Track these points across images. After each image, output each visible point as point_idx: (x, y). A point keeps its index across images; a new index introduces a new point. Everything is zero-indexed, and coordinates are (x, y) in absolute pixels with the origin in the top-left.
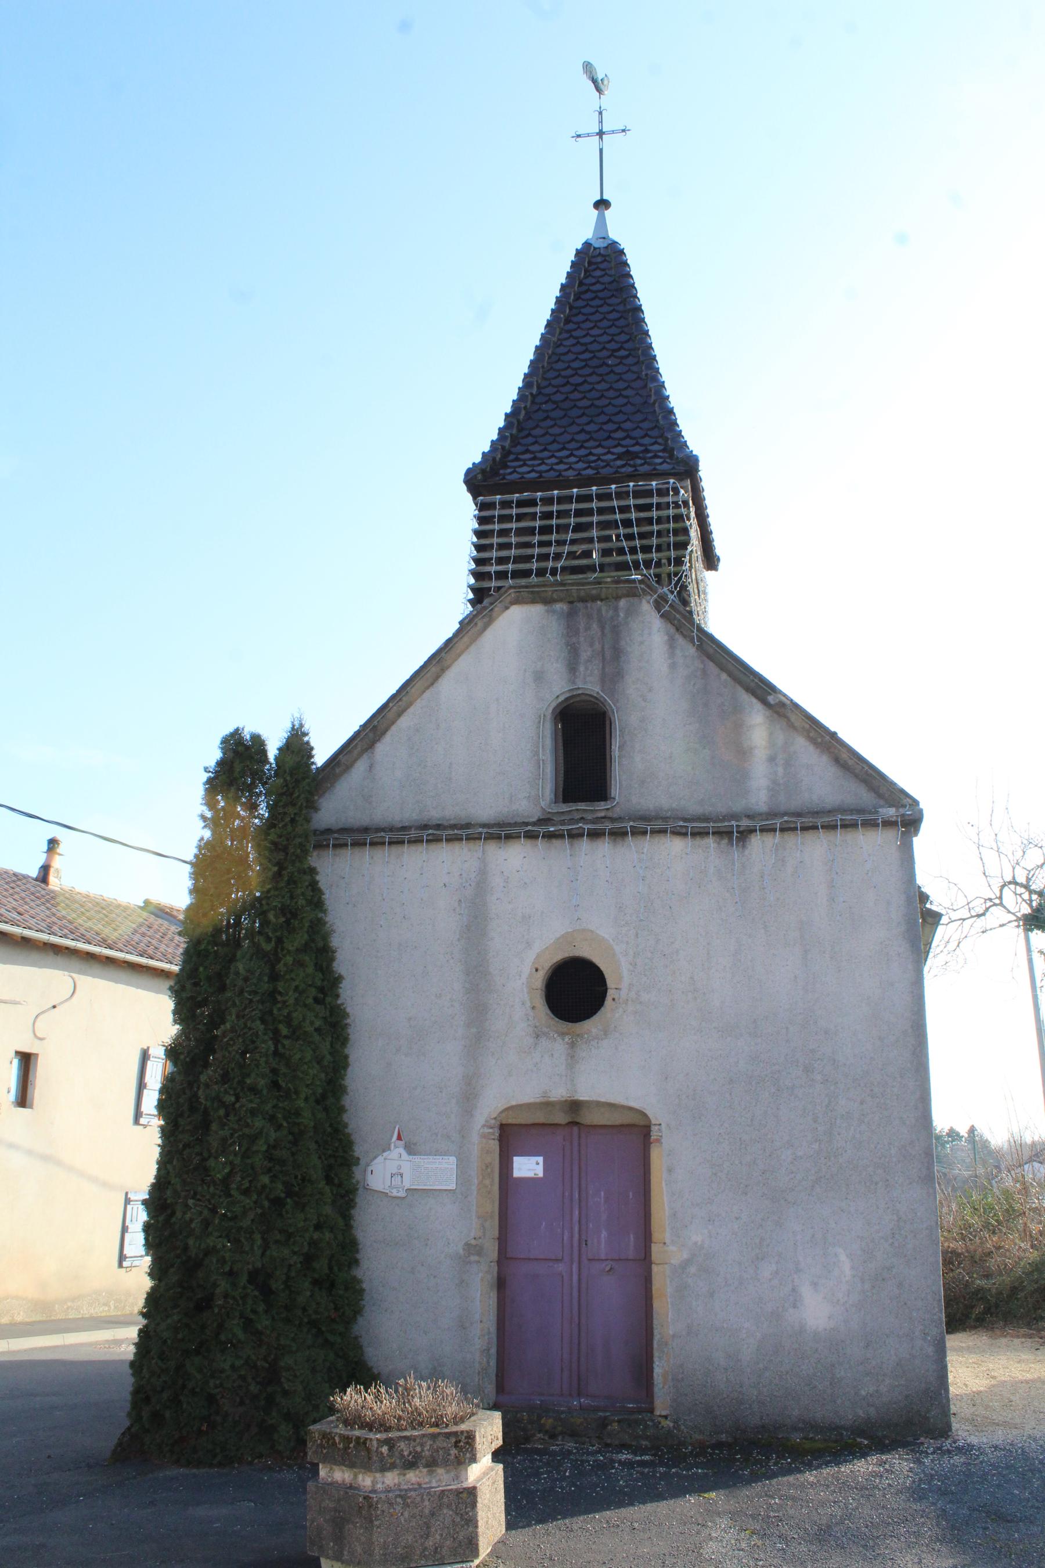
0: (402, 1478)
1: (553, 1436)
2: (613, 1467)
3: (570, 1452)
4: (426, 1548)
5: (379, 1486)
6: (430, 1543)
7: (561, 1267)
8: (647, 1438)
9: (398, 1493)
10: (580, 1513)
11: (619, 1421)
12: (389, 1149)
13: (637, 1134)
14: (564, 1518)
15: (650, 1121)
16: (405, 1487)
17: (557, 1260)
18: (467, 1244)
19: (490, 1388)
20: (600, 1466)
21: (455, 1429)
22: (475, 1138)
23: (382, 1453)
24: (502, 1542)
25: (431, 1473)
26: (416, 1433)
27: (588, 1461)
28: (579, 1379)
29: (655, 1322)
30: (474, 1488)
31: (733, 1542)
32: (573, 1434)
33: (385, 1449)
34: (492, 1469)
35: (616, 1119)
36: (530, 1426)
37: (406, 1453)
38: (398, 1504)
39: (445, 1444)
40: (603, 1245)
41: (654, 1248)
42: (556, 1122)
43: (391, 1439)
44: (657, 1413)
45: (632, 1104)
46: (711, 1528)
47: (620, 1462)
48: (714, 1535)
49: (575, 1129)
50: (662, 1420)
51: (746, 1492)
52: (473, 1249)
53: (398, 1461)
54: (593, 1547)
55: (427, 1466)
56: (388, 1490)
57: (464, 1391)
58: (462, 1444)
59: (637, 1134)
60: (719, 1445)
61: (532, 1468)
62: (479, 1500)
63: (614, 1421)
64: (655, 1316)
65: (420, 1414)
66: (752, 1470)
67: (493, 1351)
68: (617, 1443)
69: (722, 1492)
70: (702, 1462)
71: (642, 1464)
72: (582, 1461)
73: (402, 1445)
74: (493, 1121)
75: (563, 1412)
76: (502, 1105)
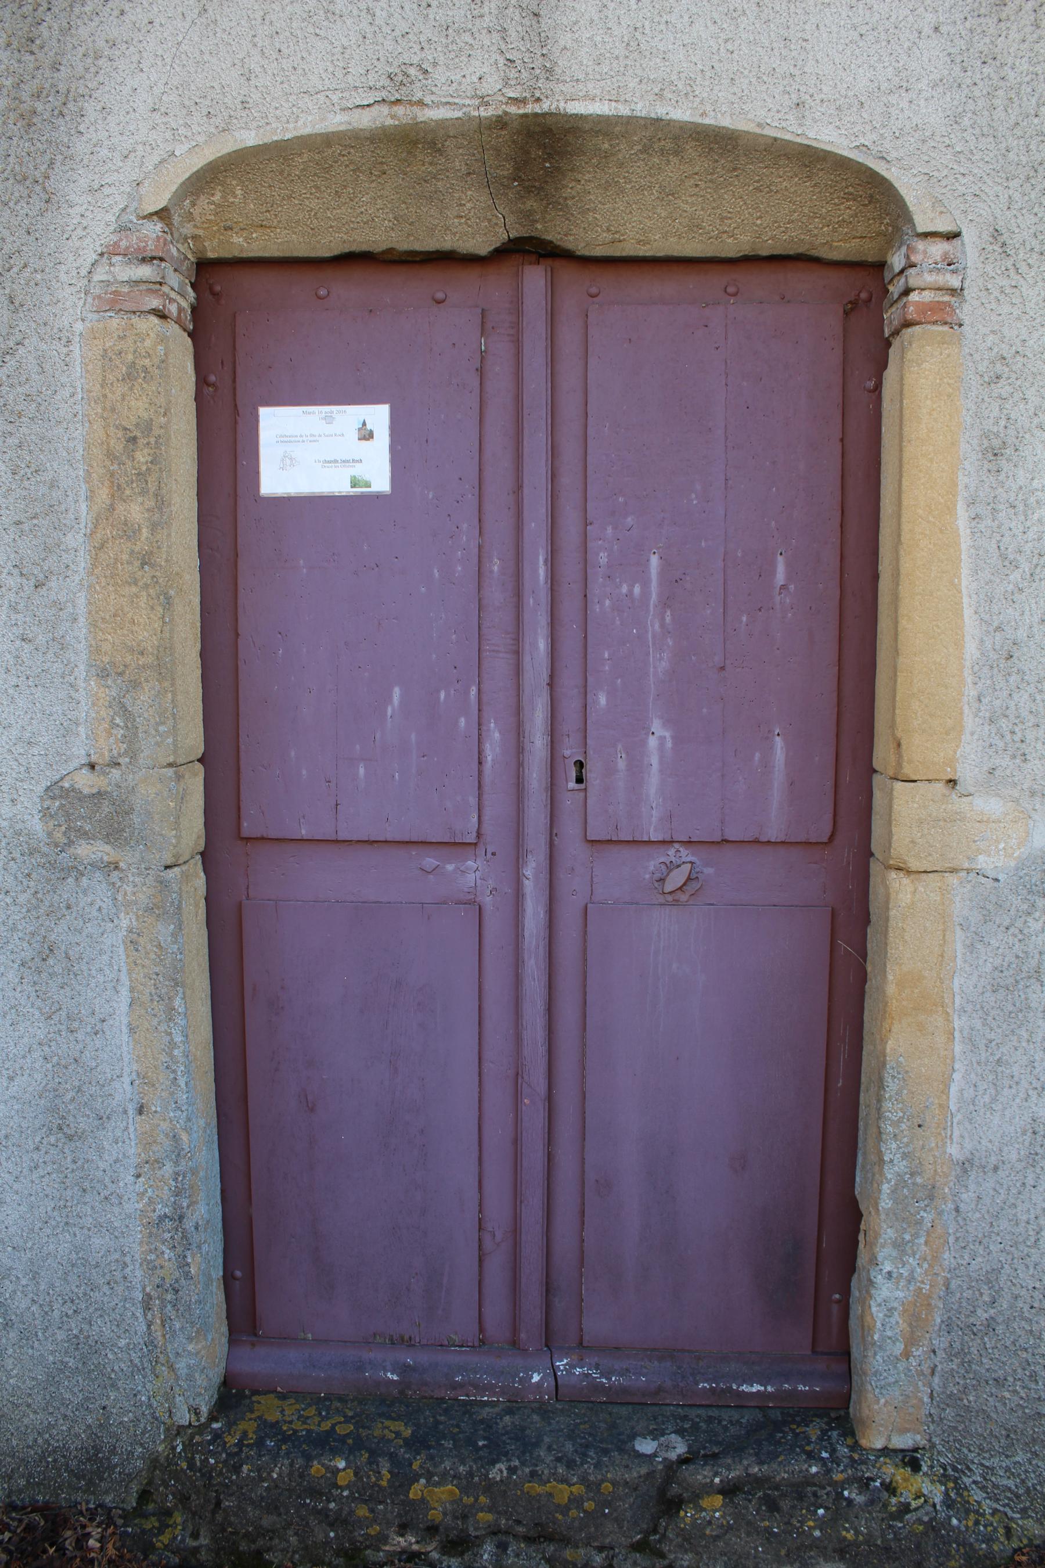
7: (472, 874)
11: (729, 1491)
17: (455, 846)
18: (56, 791)
28: (549, 1289)
36: (362, 1511)
42: (447, 243)
45: (828, 135)
49: (535, 278)
52: (87, 813)
63: (709, 1489)
74: (155, 228)
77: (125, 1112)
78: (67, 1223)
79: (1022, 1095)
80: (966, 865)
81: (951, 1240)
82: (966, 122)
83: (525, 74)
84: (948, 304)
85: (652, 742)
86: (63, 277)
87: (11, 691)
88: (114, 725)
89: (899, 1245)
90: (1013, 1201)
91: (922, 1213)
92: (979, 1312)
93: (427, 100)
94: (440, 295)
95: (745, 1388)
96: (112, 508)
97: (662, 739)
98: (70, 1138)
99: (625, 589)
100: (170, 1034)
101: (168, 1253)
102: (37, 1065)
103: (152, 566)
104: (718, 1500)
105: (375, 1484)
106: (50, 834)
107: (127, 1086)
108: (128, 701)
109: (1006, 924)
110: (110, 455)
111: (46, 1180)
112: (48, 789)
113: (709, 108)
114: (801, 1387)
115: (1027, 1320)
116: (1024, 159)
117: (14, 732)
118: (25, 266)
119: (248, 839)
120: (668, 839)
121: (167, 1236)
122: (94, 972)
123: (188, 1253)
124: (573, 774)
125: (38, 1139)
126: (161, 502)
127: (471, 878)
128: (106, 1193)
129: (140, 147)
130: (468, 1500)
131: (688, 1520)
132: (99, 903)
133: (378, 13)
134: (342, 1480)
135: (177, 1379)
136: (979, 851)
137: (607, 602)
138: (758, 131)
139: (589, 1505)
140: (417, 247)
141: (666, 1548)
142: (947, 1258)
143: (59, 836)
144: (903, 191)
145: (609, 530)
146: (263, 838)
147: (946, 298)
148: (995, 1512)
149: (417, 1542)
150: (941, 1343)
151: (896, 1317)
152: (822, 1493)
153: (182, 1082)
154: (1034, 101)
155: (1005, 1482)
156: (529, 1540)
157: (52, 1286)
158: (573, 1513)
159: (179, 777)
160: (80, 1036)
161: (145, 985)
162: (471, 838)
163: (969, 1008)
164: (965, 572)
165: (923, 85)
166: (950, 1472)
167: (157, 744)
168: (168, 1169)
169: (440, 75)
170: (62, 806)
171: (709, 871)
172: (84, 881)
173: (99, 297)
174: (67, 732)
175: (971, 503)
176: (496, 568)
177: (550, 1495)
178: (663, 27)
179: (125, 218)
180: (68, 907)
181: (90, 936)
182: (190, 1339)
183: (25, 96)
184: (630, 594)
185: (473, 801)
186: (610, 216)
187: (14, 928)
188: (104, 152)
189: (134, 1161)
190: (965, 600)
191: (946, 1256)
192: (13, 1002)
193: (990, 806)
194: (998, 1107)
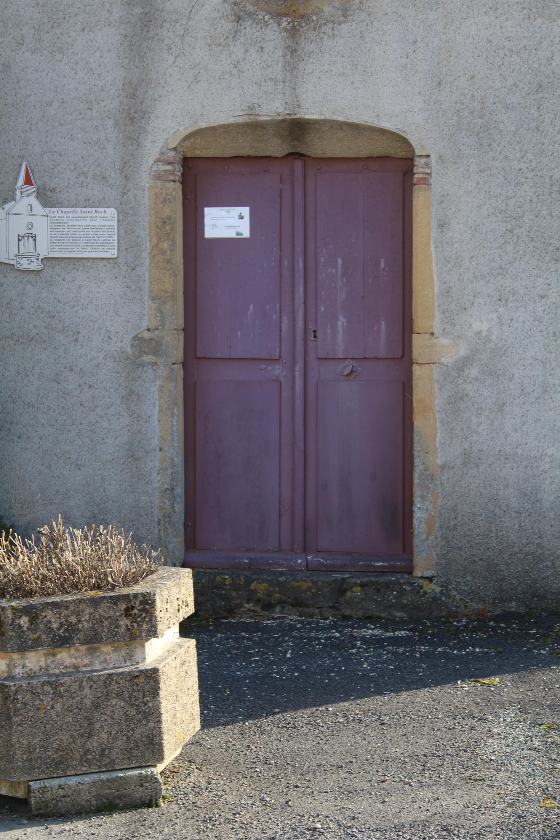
0: (51, 659)
1: (268, 607)
2: (354, 646)
3: (292, 628)
4: (89, 750)
5: (18, 670)
6: (93, 744)
7: (277, 370)
8: (403, 608)
9: (46, 679)
10: (306, 706)
11: (362, 585)
12: (14, 199)
13: (391, 171)
14: (283, 711)
15: (413, 151)
16: (56, 671)
17: (271, 360)
18: (136, 338)
19: (177, 542)
20: (335, 645)
21: (125, 591)
22: (145, 179)
23: (20, 627)
24: (195, 742)
25: (92, 651)
26: (68, 598)
27: (319, 639)
28: (305, 529)
29: (417, 447)
30: (155, 671)
31: (522, 739)
32: (298, 603)
33: (24, 621)
34: (180, 646)
35: (365, 148)
36: (234, 594)
37: (55, 626)
38: (46, 694)
39: (111, 613)
40: (340, 337)
41: (417, 341)
42: (268, 154)
43: (33, 607)
44: (418, 573)
46: (492, 722)
47: (364, 639)
48: (495, 730)
49: (298, 165)
50: (425, 583)
51: (542, 676)
53: (44, 637)
54: (325, 747)
55: (86, 642)
56: (31, 675)
57: (137, 540)
58: (135, 611)
59: (391, 171)
60: (507, 617)
61: (237, 649)
62: (162, 685)
63: (356, 584)
64: (416, 438)
65: (73, 573)
66: (552, 649)
67: (180, 490)
68: (360, 614)
69: (509, 677)
70: (482, 639)
71: (396, 641)
72: (310, 639)
73: (49, 614)
74: (172, 154)
75: (281, 574)
76: (185, 129)
77: (155, 450)
78: (133, 491)
79: (460, 441)
80: (438, 361)
81: (440, 495)
82: (430, 121)
83: (291, 107)
84: (427, 178)
85: (340, 323)
86: (143, 169)
87: (123, 304)
88: (157, 316)
89: (422, 497)
90: (459, 479)
91: (430, 485)
92: (451, 522)
93: (260, 114)
94: (266, 169)
95: (376, 564)
96: (157, 244)
97: (343, 322)
98: (136, 460)
99: (330, 270)
100: (172, 422)
101: (168, 503)
102: (125, 433)
103: (171, 263)
104: (359, 589)
105: (239, 584)
106: (133, 353)
107: (156, 441)
108: (162, 308)
109: (451, 381)
110: (157, 227)
111: (126, 475)
112: (134, 337)
113: (349, 117)
114: (397, 564)
115: (468, 525)
116: (448, 133)
117: (123, 318)
118: (131, 166)
119: (199, 358)
120: (345, 357)
121: (168, 496)
122: (147, 400)
123: (175, 503)
124: (313, 335)
125: (124, 460)
126: (174, 242)
127: (277, 372)
128: (147, 480)
129: (168, 128)
130: (271, 589)
131: (348, 596)
132: (150, 376)
133: (245, 88)
134: (227, 582)
135: (169, 552)
136: (442, 357)
137: (324, 275)
138: (365, 124)
139: (314, 590)
140: (258, 155)
141: (341, 608)
142: (440, 502)
143: (137, 354)
144: (412, 142)
145: (324, 250)
146: (204, 358)
147: (426, 176)
148: (461, 599)
149: (253, 606)
150: (439, 534)
151: (423, 525)
152: (396, 587)
153: (176, 439)
154: (451, 115)
155: (464, 588)
156: (293, 606)
157: (126, 516)
158: (308, 593)
159: (178, 334)
160: (141, 423)
161: (164, 404)
162: (277, 357)
163: (441, 410)
164: (434, 264)
165: (416, 110)
166: (444, 584)
167: (171, 322)
168: (169, 471)
169: (264, 107)
170: (138, 343)
171: (360, 369)
172: (145, 369)
173: (154, 175)
174: (141, 318)
175: (435, 242)
176: (286, 263)
177: (300, 586)
178: (334, 92)
179: (163, 150)
180: (139, 378)
181: (146, 387)
182: (174, 536)
183: (132, 112)
184: (331, 272)
185: (278, 344)
186: (320, 146)
187: (120, 385)
188: (156, 130)
189: (158, 468)
190: (434, 274)
191: (439, 501)
192: (119, 411)
193: (444, 341)
194: (452, 445)
